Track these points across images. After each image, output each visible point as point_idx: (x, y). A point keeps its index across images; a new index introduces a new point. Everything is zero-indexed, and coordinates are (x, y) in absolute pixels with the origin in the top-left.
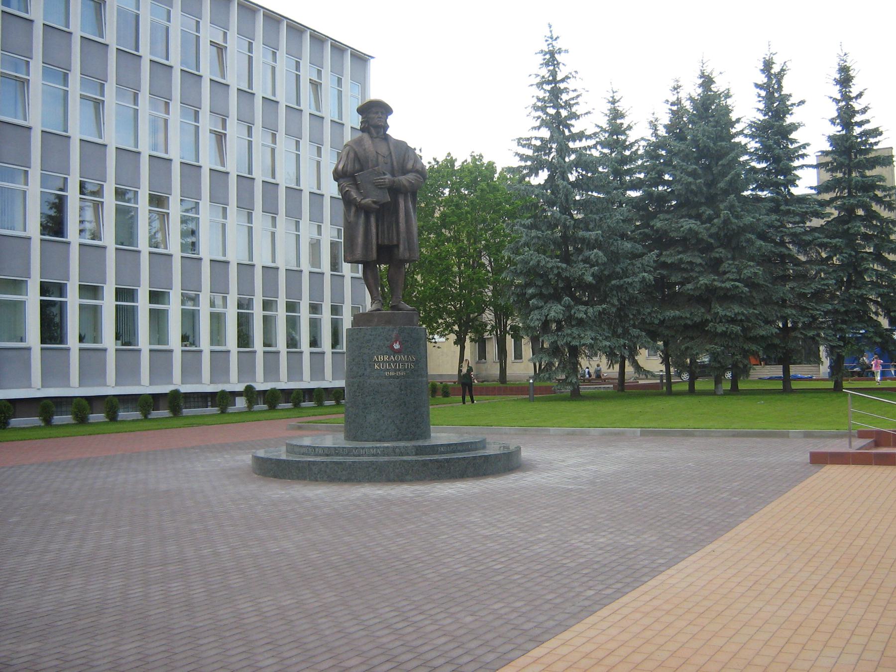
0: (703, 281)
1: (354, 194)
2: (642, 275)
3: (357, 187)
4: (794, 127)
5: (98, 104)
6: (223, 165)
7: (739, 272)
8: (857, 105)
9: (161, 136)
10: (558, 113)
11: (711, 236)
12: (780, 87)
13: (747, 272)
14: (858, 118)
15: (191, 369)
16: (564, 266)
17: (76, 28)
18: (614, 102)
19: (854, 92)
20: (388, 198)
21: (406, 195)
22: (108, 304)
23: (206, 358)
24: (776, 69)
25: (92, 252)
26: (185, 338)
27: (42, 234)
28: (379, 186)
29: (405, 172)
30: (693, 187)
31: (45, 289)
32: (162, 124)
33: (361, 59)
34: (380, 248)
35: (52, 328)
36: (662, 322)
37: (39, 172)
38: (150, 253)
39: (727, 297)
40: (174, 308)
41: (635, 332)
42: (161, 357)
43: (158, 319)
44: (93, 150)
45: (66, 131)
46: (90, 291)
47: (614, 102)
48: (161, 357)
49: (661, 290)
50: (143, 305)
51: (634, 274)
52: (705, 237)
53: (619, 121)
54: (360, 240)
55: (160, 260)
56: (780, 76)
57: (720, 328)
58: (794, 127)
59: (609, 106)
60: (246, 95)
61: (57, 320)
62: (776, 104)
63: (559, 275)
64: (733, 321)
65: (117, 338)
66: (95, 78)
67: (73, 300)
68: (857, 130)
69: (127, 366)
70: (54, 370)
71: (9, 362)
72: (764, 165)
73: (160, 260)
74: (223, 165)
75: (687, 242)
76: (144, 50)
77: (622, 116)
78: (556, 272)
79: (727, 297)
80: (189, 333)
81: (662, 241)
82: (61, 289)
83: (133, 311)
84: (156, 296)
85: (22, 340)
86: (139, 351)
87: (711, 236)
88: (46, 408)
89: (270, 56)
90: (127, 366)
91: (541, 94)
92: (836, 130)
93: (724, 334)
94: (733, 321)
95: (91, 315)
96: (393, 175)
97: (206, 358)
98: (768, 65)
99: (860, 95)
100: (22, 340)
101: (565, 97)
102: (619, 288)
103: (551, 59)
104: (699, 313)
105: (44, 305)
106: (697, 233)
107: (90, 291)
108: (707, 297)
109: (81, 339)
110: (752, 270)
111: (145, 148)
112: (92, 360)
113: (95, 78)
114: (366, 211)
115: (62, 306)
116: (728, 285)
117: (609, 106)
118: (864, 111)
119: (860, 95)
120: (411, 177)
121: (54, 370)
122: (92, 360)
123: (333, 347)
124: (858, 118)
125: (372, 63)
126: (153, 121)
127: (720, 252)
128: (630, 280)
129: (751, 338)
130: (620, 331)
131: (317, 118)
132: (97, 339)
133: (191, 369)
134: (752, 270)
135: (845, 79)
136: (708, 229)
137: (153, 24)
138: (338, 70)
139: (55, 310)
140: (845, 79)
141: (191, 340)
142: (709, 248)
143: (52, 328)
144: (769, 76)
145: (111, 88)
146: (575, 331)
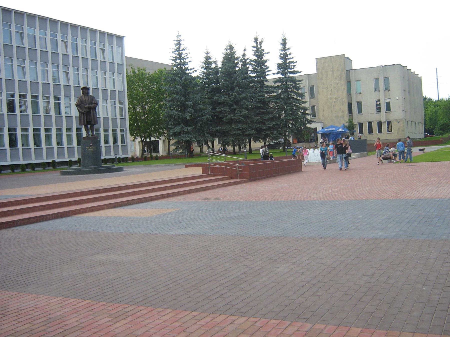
0: (228, 117)
1: (80, 110)
2: (207, 114)
3: (81, 108)
4: (266, 61)
5: (23, 68)
6: (69, 83)
7: (241, 113)
8: (288, 52)
9: (46, 75)
10: (181, 61)
11: (231, 101)
12: (261, 47)
13: (243, 113)
14: (289, 57)
15: (61, 153)
16: (180, 114)
17: (14, 44)
18: (207, 53)
19: (287, 47)
20: (88, 110)
21: (93, 109)
22: (31, 133)
23: (66, 150)
24: (259, 41)
25: (24, 117)
26: (58, 143)
27: (3, 135)
28: (86, 108)
29: (92, 104)
30: (225, 85)
31: (10, 130)
32: (46, 72)
33: (120, 38)
34: (87, 122)
35: (13, 142)
36: (217, 131)
37: (5, 92)
38: (44, 116)
39: (238, 122)
40: (54, 133)
41: (207, 135)
42: (50, 150)
43: (48, 137)
44: (23, 83)
45: (13, 78)
46: (25, 130)
47: (207, 53)
48: (50, 150)
49: (217, 120)
50: (43, 133)
51: (205, 116)
52: (229, 102)
53: (209, 60)
54: (82, 120)
55: (48, 117)
56: (261, 43)
57: (234, 132)
58: (266, 61)
59: (206, 55)
60: (75, 58)
61: (14, 139)
62: (259, 53)
63: (179, 117)
64: (239, 130)
65: (34, 145)
66: (22, 59)
67: (19, 133)
68: (288, 61)
69: (38, 153)
70: (14, 156)
71: (1, 153)
72: (256, 75)
73: (48, 117)
74: (69, 83)
75: (223, 103)
76: (38, 47)
77: (210, 58)
78: (177, 116)
79: (238, 122)
80: (59, 141)
81: (215, 104)
82: (15, 130)
83: (39, 135)
84: (47, 130)
85: (3, 147)
86: (42, 148)
87: (231, 101)
88: (13, 168)
89: (84, 42)
90: (38, 153)
91: (174, 55)
92: (281, 61)
93: (235, 134)
94: (239, 130)
95: (25, 138)
96: (89, 104)
97: (66, 150)
98: (256, 40)
99: (289, 49)
100: (3, 147)
101: (183, 56)
102: (201, 120)
103: (179, 43)
104: (228, 127)
105: (10, 135)
106: (226, 101)
107: (25, 130)
108: (231, 122)
109: (23, 145)
110: (244, 112)
111: (40, 80)
112: (27, 153)
113: (22, 59)
114: (82, 113)
115: (16, 135)
116: (236, 118)
117: (206, 55)
118: (290, 54)
119: (289, 49)
120: (93, 105)
121: (14, 156)
122: (27, 153)
123: (114, 144)
124: (289, 57)
125: (125, 39)
126: (43, 71)
127: (235, 107)
128: (203, 118)
129: (246, 135)
130: (202, 134)
131: (103, 62)
132: (28, 145)
133: (61, 153)
134: (244, 112)
135: (284, 43)
136: (230, 99)
137: (40, 38)
138: (111, 43)
139: (13, 137)
140: (284, 43)
141: (60, 144)
142: (231, 106)
143: (13, 142)
144: (257, 43)
145: (27, 62)
146: (185, 136)
